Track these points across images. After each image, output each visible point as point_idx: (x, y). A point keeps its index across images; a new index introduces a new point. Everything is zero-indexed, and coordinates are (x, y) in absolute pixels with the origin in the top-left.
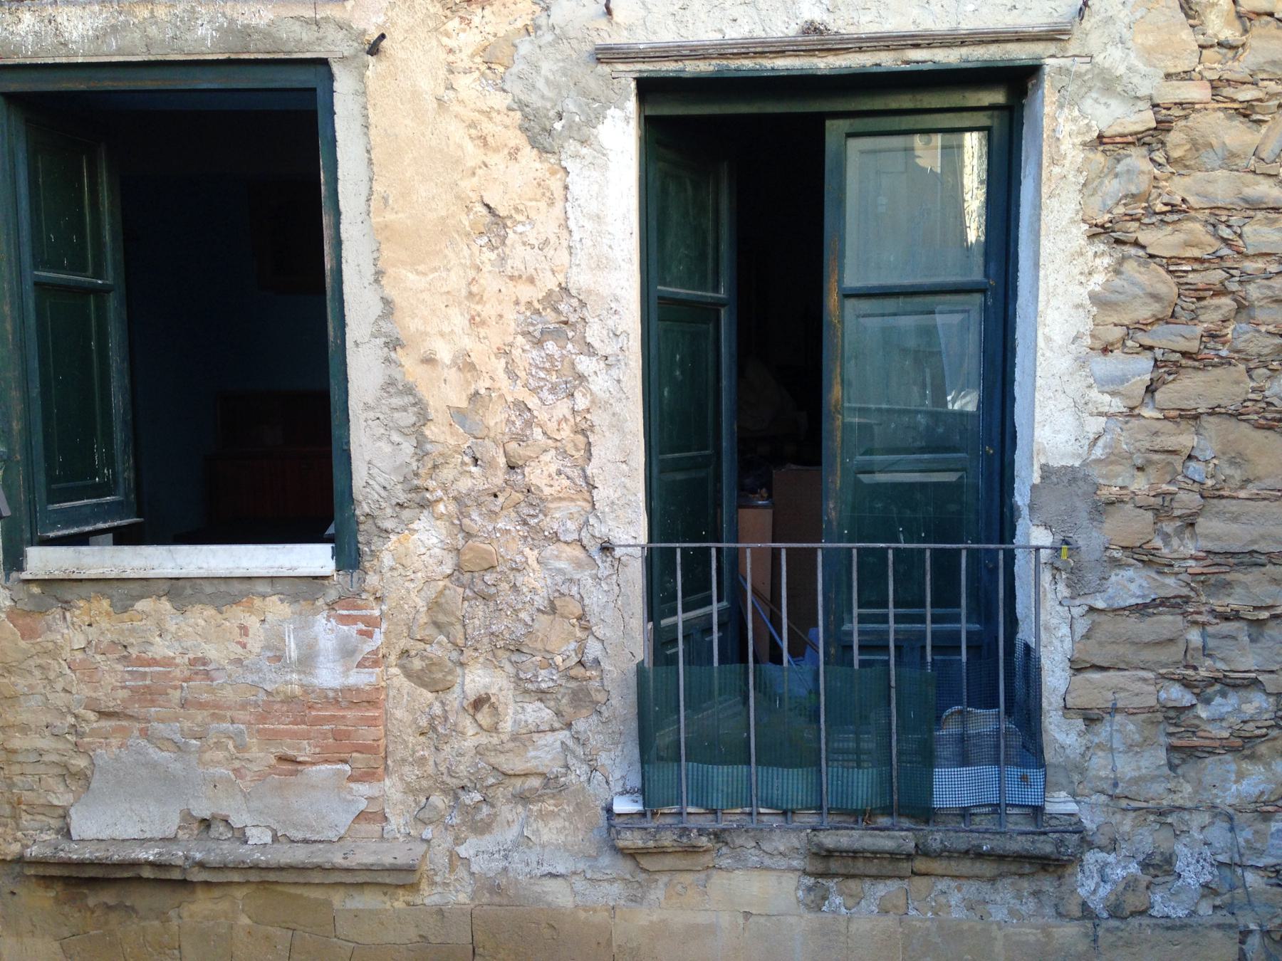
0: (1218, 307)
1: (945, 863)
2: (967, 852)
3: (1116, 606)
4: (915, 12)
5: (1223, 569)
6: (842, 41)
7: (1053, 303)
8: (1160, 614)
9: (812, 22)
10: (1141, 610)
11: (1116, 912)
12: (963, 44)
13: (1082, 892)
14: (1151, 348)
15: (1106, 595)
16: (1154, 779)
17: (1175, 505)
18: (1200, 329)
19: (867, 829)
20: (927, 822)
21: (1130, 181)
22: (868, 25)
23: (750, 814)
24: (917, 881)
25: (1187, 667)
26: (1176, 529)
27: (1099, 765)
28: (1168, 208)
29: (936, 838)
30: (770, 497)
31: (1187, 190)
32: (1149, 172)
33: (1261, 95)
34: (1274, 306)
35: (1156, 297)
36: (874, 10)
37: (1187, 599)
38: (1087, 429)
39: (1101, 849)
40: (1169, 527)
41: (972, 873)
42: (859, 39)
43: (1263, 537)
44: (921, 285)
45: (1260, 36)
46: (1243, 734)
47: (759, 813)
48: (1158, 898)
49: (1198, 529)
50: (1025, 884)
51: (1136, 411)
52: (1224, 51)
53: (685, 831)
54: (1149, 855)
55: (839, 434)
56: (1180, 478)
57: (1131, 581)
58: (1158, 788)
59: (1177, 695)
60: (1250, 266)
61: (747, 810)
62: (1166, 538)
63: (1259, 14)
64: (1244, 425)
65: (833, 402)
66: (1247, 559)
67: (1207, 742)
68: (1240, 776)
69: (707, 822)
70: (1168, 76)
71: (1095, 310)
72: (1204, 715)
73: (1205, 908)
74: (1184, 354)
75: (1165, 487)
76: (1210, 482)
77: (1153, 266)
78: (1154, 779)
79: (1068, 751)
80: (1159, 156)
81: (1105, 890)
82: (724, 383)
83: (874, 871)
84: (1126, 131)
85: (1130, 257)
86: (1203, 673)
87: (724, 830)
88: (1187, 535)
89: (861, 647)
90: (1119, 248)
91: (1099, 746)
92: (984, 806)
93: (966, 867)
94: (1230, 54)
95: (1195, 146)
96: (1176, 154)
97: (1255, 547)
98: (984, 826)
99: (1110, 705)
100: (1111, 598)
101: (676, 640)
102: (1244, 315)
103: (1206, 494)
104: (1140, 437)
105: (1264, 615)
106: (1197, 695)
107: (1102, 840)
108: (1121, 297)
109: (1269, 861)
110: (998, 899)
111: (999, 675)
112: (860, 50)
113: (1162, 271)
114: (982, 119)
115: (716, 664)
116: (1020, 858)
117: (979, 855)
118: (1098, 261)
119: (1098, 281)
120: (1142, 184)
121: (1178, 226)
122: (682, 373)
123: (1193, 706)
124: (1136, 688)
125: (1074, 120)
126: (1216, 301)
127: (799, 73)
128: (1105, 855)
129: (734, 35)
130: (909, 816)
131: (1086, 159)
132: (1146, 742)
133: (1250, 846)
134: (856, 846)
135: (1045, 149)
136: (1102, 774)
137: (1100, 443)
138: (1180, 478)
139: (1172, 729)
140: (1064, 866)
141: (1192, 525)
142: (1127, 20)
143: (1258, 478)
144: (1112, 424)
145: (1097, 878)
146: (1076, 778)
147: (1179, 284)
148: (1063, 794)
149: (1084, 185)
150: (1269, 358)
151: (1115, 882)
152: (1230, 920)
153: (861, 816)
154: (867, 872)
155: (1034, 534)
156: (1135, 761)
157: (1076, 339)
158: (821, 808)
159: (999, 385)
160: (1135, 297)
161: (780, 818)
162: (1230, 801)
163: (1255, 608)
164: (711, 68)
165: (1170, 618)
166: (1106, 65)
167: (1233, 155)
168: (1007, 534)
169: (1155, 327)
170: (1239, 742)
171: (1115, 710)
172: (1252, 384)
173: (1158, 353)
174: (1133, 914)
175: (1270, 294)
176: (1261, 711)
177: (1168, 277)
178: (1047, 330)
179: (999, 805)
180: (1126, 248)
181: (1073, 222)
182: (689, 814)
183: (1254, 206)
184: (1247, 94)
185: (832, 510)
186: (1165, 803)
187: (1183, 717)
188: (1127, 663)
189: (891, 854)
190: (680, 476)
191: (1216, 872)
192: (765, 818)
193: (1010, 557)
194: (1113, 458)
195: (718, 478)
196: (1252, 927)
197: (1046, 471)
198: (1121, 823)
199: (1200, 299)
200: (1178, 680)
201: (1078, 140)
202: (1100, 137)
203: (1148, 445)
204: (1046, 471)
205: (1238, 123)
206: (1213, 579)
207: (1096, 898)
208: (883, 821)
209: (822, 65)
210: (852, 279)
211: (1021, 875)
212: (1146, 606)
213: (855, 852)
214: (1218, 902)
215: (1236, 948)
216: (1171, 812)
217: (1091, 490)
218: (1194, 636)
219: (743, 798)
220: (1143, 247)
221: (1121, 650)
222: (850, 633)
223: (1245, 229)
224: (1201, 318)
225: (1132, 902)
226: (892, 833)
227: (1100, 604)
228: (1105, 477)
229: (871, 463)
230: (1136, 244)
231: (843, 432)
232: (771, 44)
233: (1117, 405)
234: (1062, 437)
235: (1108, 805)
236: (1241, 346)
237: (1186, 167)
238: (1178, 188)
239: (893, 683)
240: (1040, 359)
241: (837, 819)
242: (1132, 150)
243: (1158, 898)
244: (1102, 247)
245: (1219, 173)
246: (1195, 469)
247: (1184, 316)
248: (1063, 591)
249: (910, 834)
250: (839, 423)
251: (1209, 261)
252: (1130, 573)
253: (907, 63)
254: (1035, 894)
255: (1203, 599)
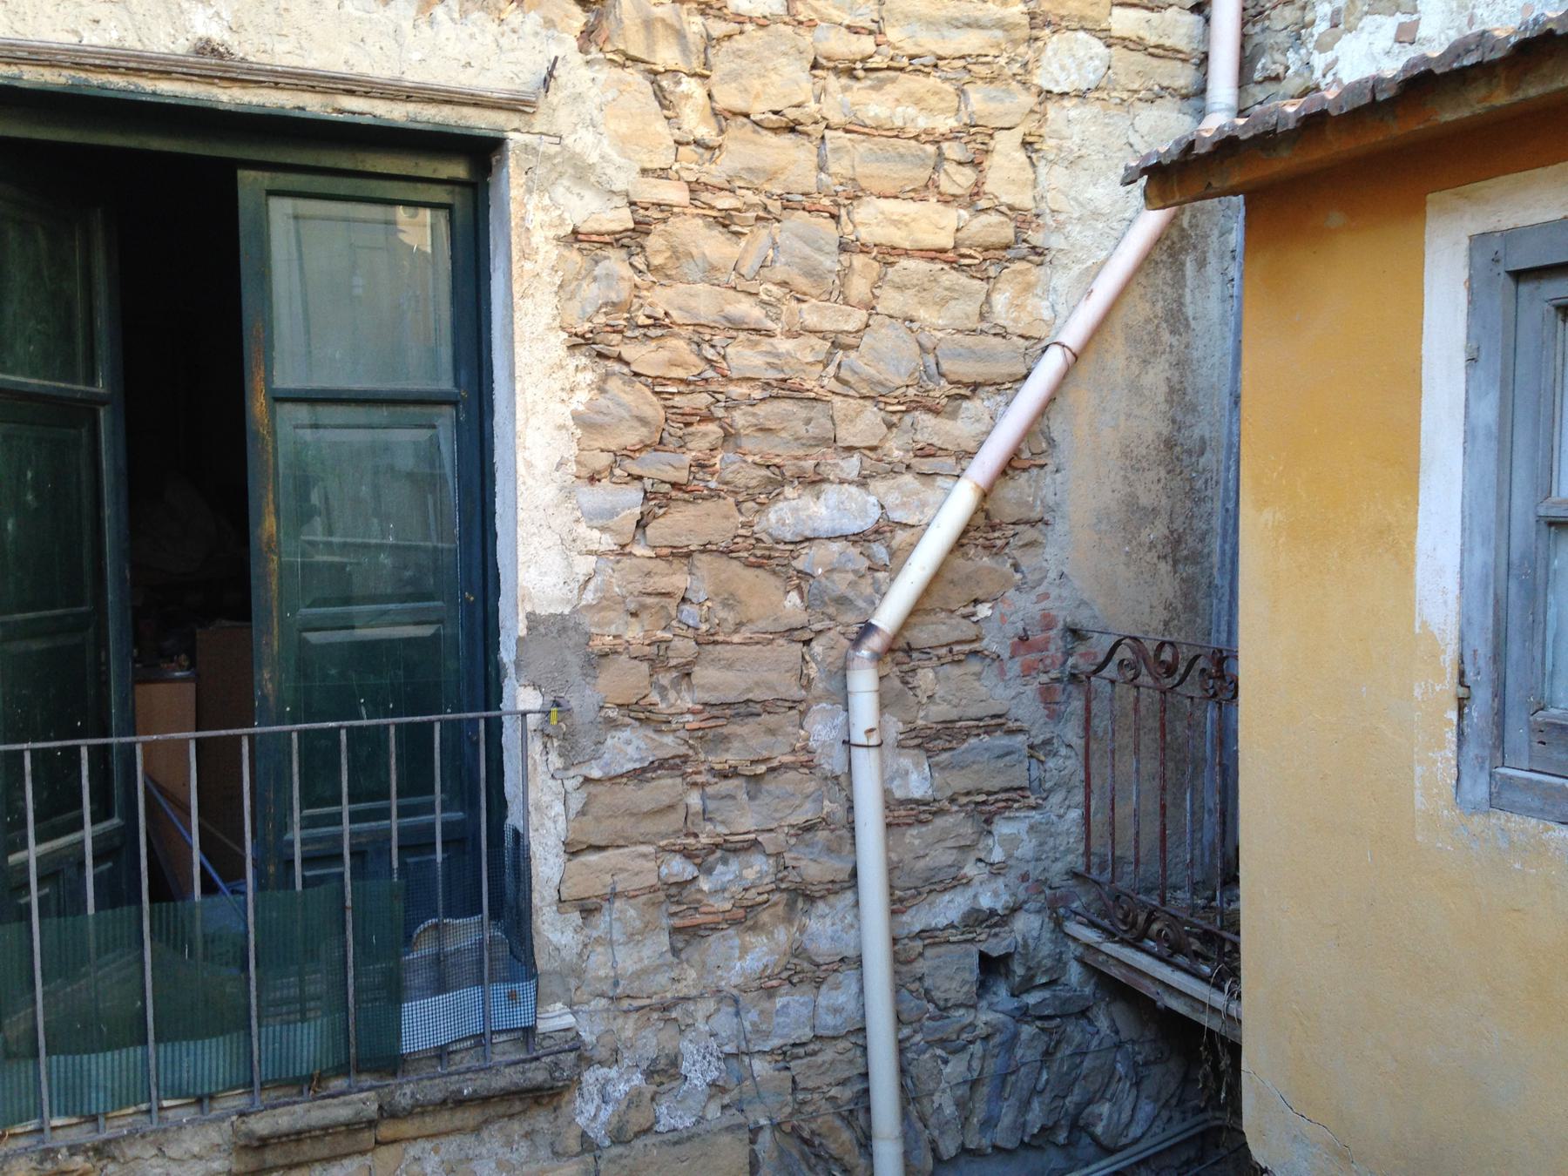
0: (705, 434)
1: (417, 1122)
2: (444, 1102)
3: (613, 773)
4: (347, 50)
5: (720, 722)
6: (250, 70)
7: (533, 421)
8: (659, 778)
9: (208, 41)
10: (638, 775)
11: (619, 1137)
12: (409, 99)
13: (581, 1120)
14: (640, 478)
15: (602, 762)
16: (657, 969)
17: (670, 653)
18: (688, 458)
19: (314, 1099)
20: (394, 1074)
21: (609, 287)
22: (284, 55)
23: (149, 1111)
24: (384, 1152)
25: (687, 835)
26: (672, 682)
27: (599, 965)
28: (651, 321)
29: (405, 1092)
30: (192, 665)
31: (669, 302)
32: (630, 279)
33: (738, 204)
34: (759, 434)
35: (643, 421)
36: (292, 38)
37: (685, 759)
38: (576, 569)
39: (601, 1063)
40: (665, 679)
41: (451, 1126)
42: (274, 72)
43: (757, 684)
44: (376, 392)
45: (736, 138)
46: (745, 903)
47: (161, 1109)
48: (664, 1110)
49: (695, 679)
50: (516, 1127)
51: (628, 550)
52: (701, 150)
53: (49, 1154)
54: (654, 1061)
55: (274, 582)
56: (674, 623)
57: (628, 742)
58: (663, 979)
59: (678, 868)
60: (736, 391)
61: (144, 1107)
62: (663, 690)
63: (735, 114)
64: (735, 563)
65: (265, 537)
66: (743, 709)
67: (710, 918)
68: (744, 951)
69: (84, 1135)
70: (644, 171)
71: (579, 432)
72: (706, 887)
73: (713, 1111)
74: (674, 485)
75: (660, 634)
76: (704, 627)
77: (638, 385)
78: (657, 969)
79: (563, 953)
80: (639, 261)
81: (607, 1113)
82: (108, 512)
83: (326, 1152)
84: (603, 229)
85: (614, 374)
86: (704, 840)
87: (108, 1142)
88: (684, 686)
89: (305, 861)
90: (602, 362)
91: (597, 940)
92: (465, 1039)
93: (444, 1120)
94: (707, 155)
95: (675, 254)
96: (657, 261)
97: (750, 696)
98: (465, 1065)
99: (608, 890)
100: (607, 764)
101: (27, 885)
102: (731, 444)
103: (700, 640)
104: (632, 578)
105: (762, 769)
106: (699, 866)
107: (602, 1053)
108: (607, 419)
109: (776, 1042)
110: (484, 1151)
111: (484, 872)
112: (276, 86)
113: (648, 392)
114: (440, 194)
115: (91, 910)
116: (507, 1095)
117: (459, 1102)
118: (580, 376)
119: (582, 398)
120: (622, 292)
121: (662, 343)
122: (36, 497)
123: (695, 878)
124: (636, 866)
125: (545, 209)
126: (704, 427)
127: (193, 103)
128: (606, 1070)
129: (95, 41)
130: (368, 1071)
131: (560, 256)
132: (648, 928)
133: (756, 1030)
134: (300, 1125)
135: (514, 239)
136: (602, 973)
137: (591, 586)
138: (674, 623)
139: (674, 909)
140: (559, 1094)
141: (688, 675)
142: (597, 100)
143: (750, 621)
144: (602, 565)
145: (597, 1100)
146: (573, 983)
147: (666, 407)
148: (559, 1005)
149: (561, 286)
150: (757, 491)
151: (617, 1101)
152: (740, 1119)
153: (308, 1084)
154: (317, 1155)
155: (522, 697)
156: (632, 952)
157: (560, 465)
158: (251, 1083)
159: (478, 519)
160: (621, 419)
161: (193, 1110)
162: (735, 980)
163: (752, 762)
164: (62, 80)
165: (670, 781)
166: (578, 150)
167: (714, 268)
168: (493, 700)
169: (643, 454)
170: (741, 913)
171: (615, 895)
172: (742, 519)
173: (648, 483)
174: (637, 1135)
175: (754, 421)
176: (761, 875)
177: (654, 399)
178: (527, 454)
179: (483, 1034)
180: (609, 363)
181: (550, 329)
182: (54, 1129)
183: (736, 326)
184: (724, 202)
185: (268, 681)
186: (669, 995)
187: (685, 893)
188: (626, 839)
189: (347, 1125)
190: (36, 645)
191: (723, 1066)
192: (170, 1114)
193: (495, 728)
194: (605, 603)
195: (101, 643)
196: (763, 1122)
197: (532, 618)
198: (623, 1028)
199: (687, 425)
200: (679, 851)
201: (551, 233)
202: (575, 232)
203: (640, 587)
204: (533, 620)
205: (717, 232)
206: (711, 734)
207: (597, 1124)
208: (338, 1084)
209: (225, 98)
210: (287, 376)
211: (511, 1116)
212: (644, 770)
213: (299, 1133)
214: (726, 1100)
215: (747, 1150)
216: (675, 1005)
217: (583, 641)
218: (694, 799)
219: (138, 1091)
220: (627, 364)
221: (619, 823)
222: (291, 844)
223: (729, 350)
224: (690, 446)
225: (638, 1120)
226: (347, 1098)
227: (596, 773)
228: (598, 625)
229: (350, 616)
230: (619, 359)
231: (280, 578)
232: (150, 60)
233: (608, 542)
234: (550, 580)
235: (608, 1010)
236: (729, 477)
237: (668, 277)
238: (661, 300)
239: (349, 903)
240: (521, 488)
241: (273, 1094)
242: (610, 252)
243: (664, 1110)
244: (584, 361)
245: (700, 286)
246: (690, 613)
247: (672, 443)
248: (556, 761)
249: (372, 1094)
250: (274, 566)
251: (694, 383)
252: (626, 734)
253: (341, 111)
254: (527, 1135)
255: (702, 757)
